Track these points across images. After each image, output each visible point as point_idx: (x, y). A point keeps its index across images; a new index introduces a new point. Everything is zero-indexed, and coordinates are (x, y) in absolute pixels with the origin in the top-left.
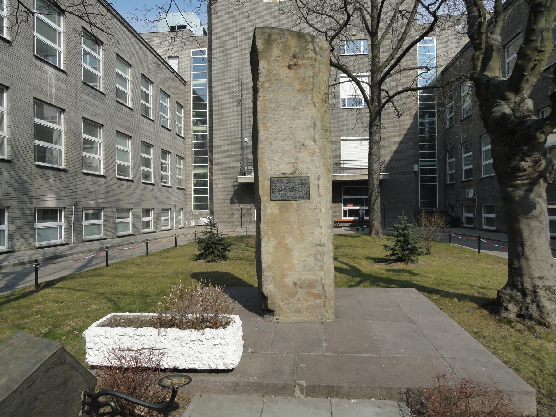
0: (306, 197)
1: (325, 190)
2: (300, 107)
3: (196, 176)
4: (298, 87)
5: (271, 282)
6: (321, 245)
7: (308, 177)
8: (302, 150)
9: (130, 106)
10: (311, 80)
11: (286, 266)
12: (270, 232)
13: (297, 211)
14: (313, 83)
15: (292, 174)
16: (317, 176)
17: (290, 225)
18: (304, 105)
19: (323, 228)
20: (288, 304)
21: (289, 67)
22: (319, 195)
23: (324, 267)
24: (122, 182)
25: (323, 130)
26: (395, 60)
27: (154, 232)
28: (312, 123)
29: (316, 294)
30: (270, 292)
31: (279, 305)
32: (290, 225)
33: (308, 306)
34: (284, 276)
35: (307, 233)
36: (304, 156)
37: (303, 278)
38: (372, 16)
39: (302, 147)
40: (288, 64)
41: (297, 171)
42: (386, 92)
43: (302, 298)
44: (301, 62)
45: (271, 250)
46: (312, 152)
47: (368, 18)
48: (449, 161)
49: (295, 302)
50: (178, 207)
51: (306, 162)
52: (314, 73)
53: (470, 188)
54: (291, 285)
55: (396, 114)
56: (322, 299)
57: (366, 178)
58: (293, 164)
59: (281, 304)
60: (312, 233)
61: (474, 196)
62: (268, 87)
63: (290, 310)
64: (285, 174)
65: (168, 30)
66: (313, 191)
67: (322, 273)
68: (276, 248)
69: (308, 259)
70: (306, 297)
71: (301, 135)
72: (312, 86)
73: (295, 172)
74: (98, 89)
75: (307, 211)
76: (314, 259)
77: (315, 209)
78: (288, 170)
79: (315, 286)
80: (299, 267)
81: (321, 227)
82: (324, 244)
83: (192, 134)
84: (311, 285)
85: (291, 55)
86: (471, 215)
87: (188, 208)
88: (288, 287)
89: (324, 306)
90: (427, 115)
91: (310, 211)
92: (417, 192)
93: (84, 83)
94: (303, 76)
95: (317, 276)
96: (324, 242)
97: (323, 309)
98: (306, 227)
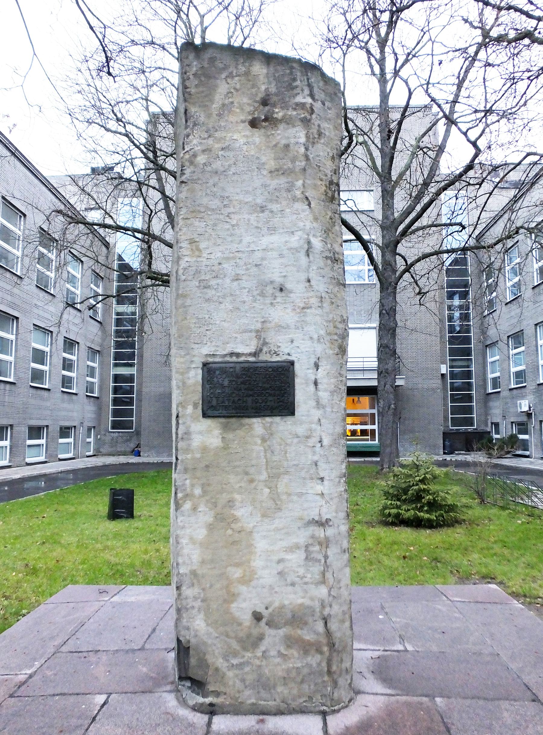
0: (286, 408)
1: (332, 393)
2: (275, 207)
3: (117, 378)
4: (272, 164)
5: (199, 610)
6: (323, 524)
7: (292, 363)
8: (279, 300)
9: (18, 274)
10: (302, 150)
11: (236, 573)
12: (198, 491)
13: (264, 440)
14: (307, 158)
15: (255, 354)
16: (313, 360)
17: (247, 473)
18: (284, 203)
19: (326, 482)
20: (240, 666)
21: (254, 124)
22: (319, 405)
23: (329, 575)
24: (39, 392)
25: (327, 258)
26: (418, 208)
27: (45, 462)
28: (302, 242)
29: (310, 644)
30: (196, 636)
31: (217, 669)
32: (247, 473)
33: (288, 671)
34: (232, 597)
35: (289, 495)
36: (281, 314)
37: (277, 604)
38: (381, 151)
39: (278, 294)
40: (250, 118)
41: (265, 349)
42: (403, 257)
43: (273, 653)
44: (279, 113)
45: (201, 533)
46: (302, 305)
47: (377, 154)
48: (490, 360)
49: (258, 662)
50: (87, 424)
51: (288, 327)
52: (307, 137)
53: (523, 397)
54: (247, 618)
55: (417, 290)
56: (321, 653)
57: (375, 383)
58: (257, 331)
59: (220, 663)
60: (300, 495)
61: (530, 410)
62: (205, 164)
63: (243, 680)
64: (238, 355)
65: (89, 171)
66: (302, 394)
67: (323, 591)
68: (211, 527)
69: (289, 557)
70: (283, 651)
71: (275, 271)
72: (303, 163)
73: (261, 350)
74: (15, 272)
75: (289, 441)
76: (303, 556)
77: (308, 437)
78: (245, 347)
79: (306, 623)
80: (267, 576)
81: (322, 479)
82: (328, 521)
83: (114, 317)
84: (297, 618)
85: (258, 99)
86: (521, 437)
87: (102, 427)
88: (240, 624)
89: (329, 672)
90: (457, 297)
91: (296, 440)
92: (445, 405)
93: (37, 286)
94: (284, 142)
95: (312, 599)
96: (328, 516)
97: (326, 678)
98: (285, 479)
